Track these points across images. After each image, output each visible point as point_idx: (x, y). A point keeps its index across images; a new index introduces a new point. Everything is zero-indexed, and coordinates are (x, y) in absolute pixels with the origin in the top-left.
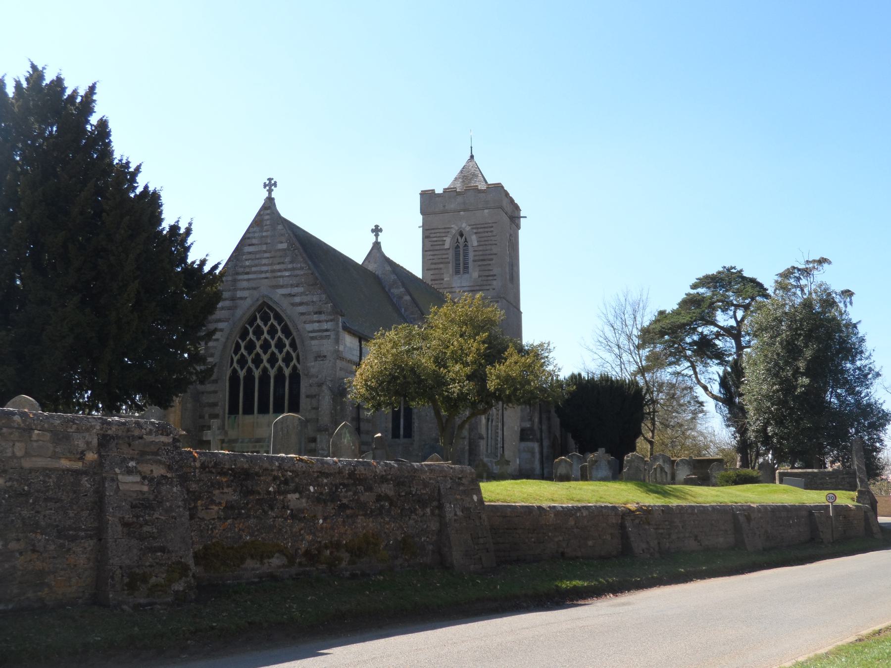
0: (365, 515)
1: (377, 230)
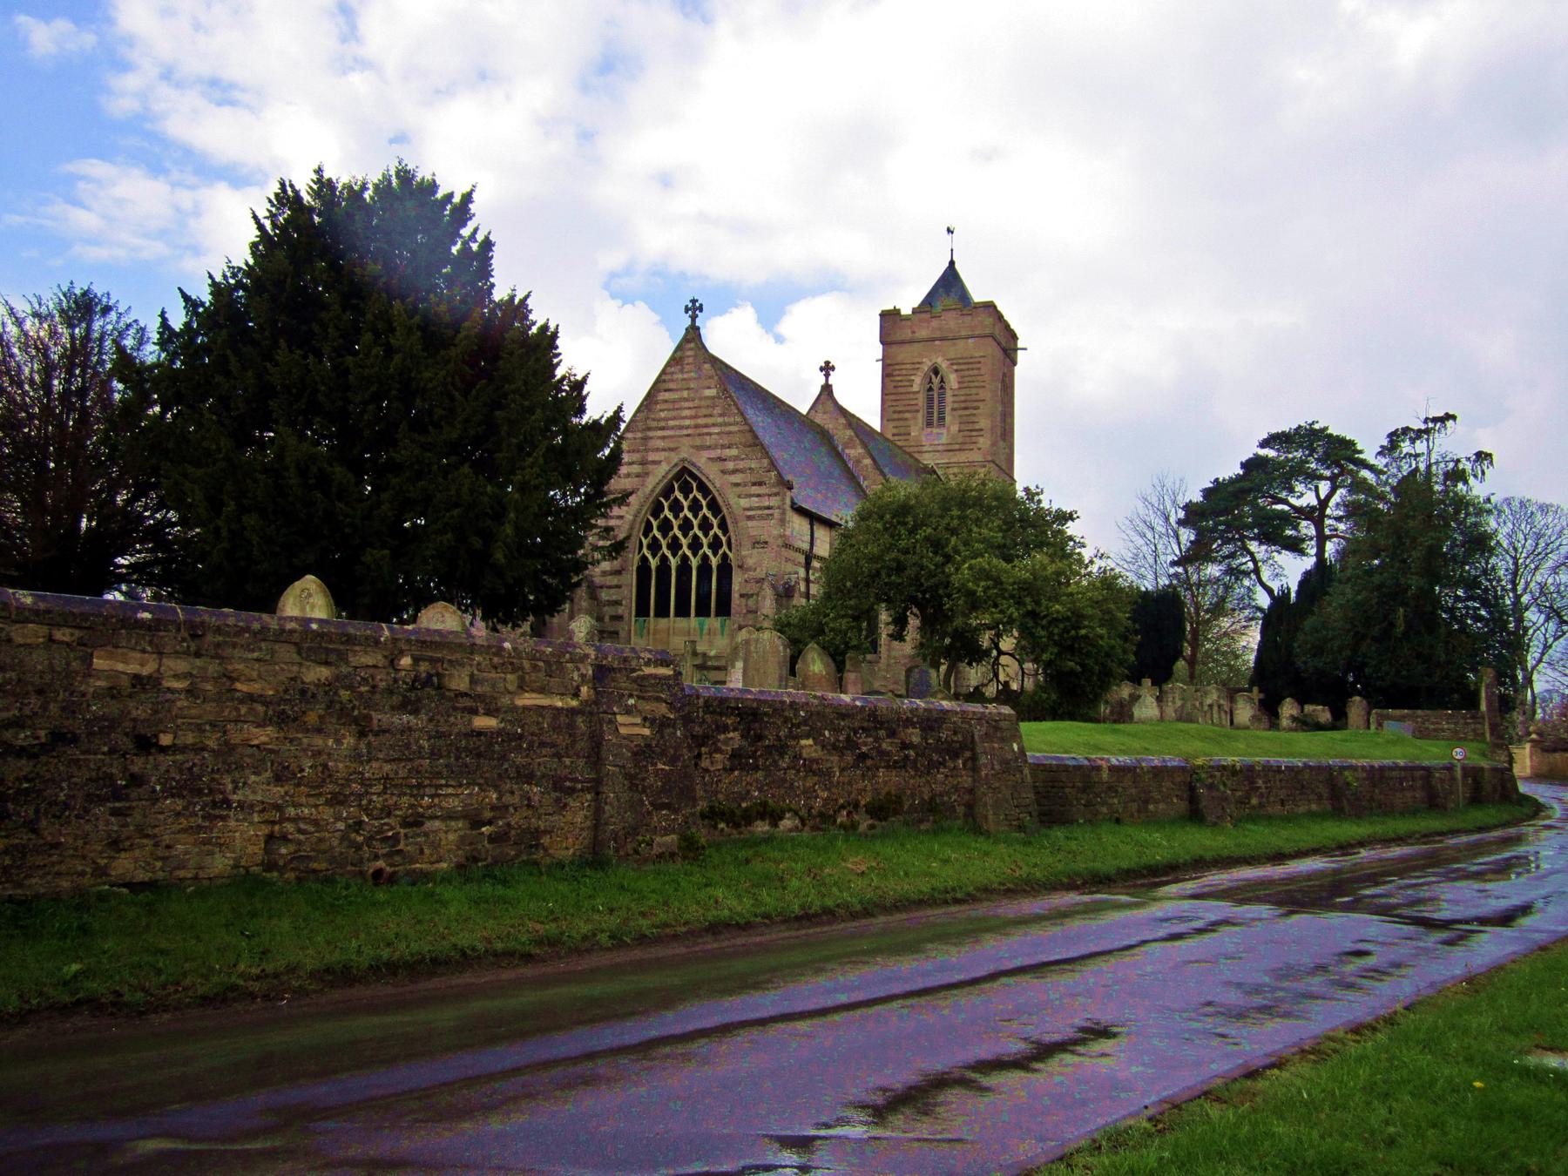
0: (887, 767)
1: (827, 368)
